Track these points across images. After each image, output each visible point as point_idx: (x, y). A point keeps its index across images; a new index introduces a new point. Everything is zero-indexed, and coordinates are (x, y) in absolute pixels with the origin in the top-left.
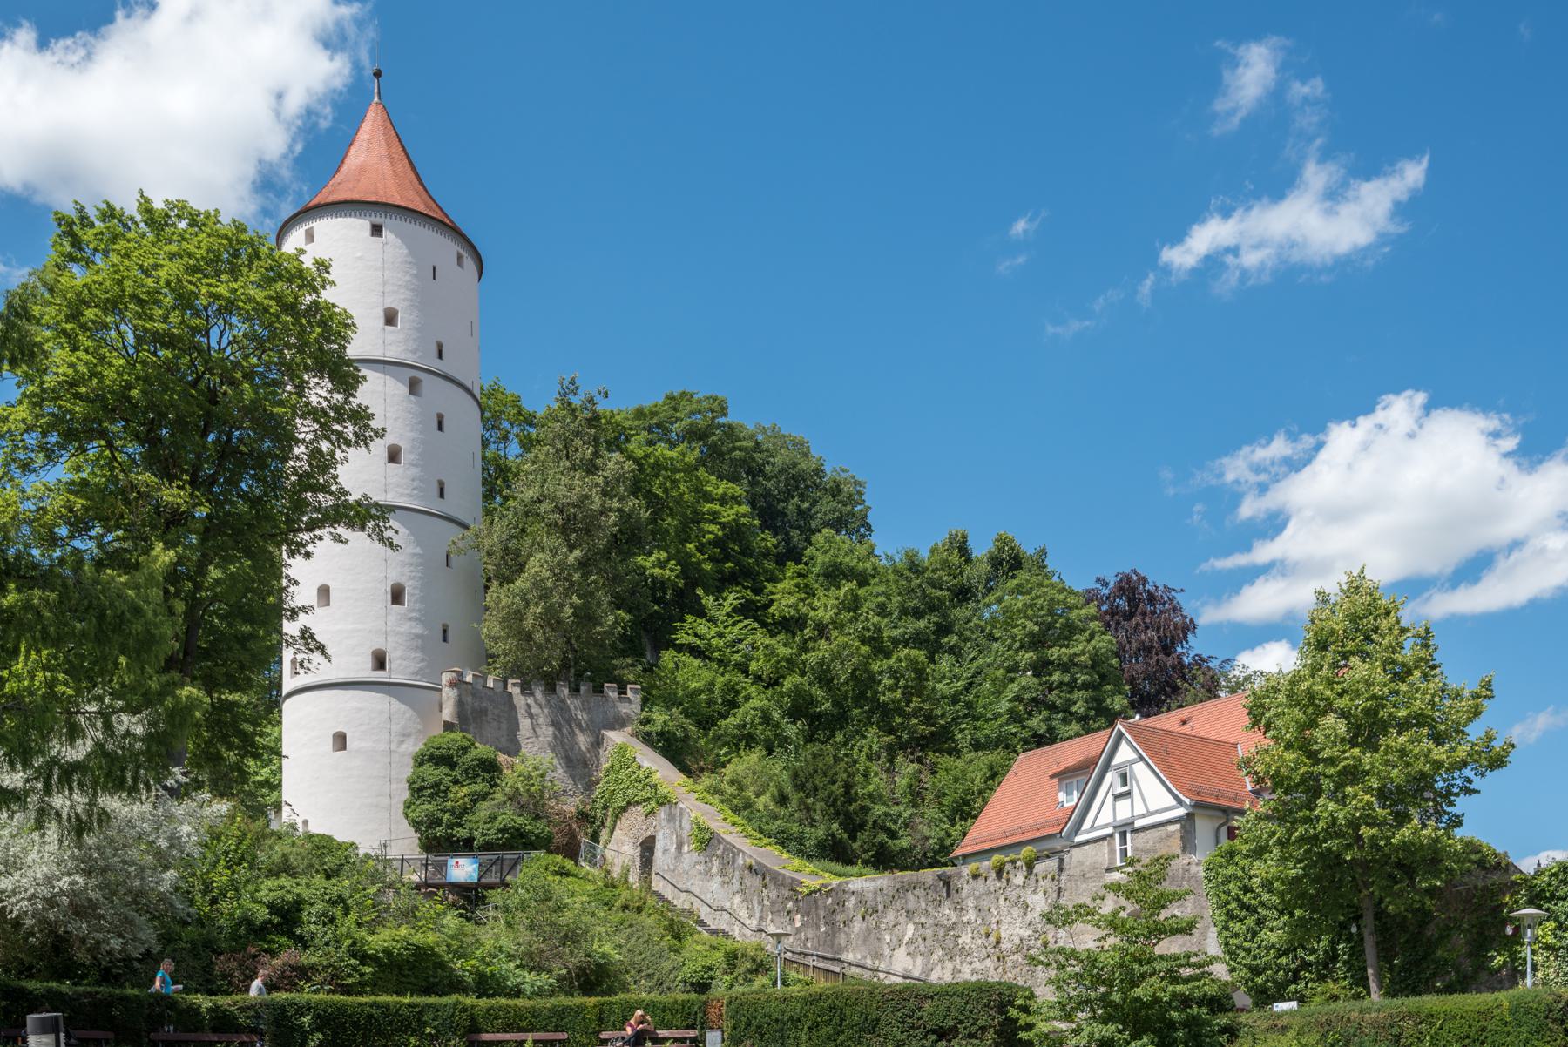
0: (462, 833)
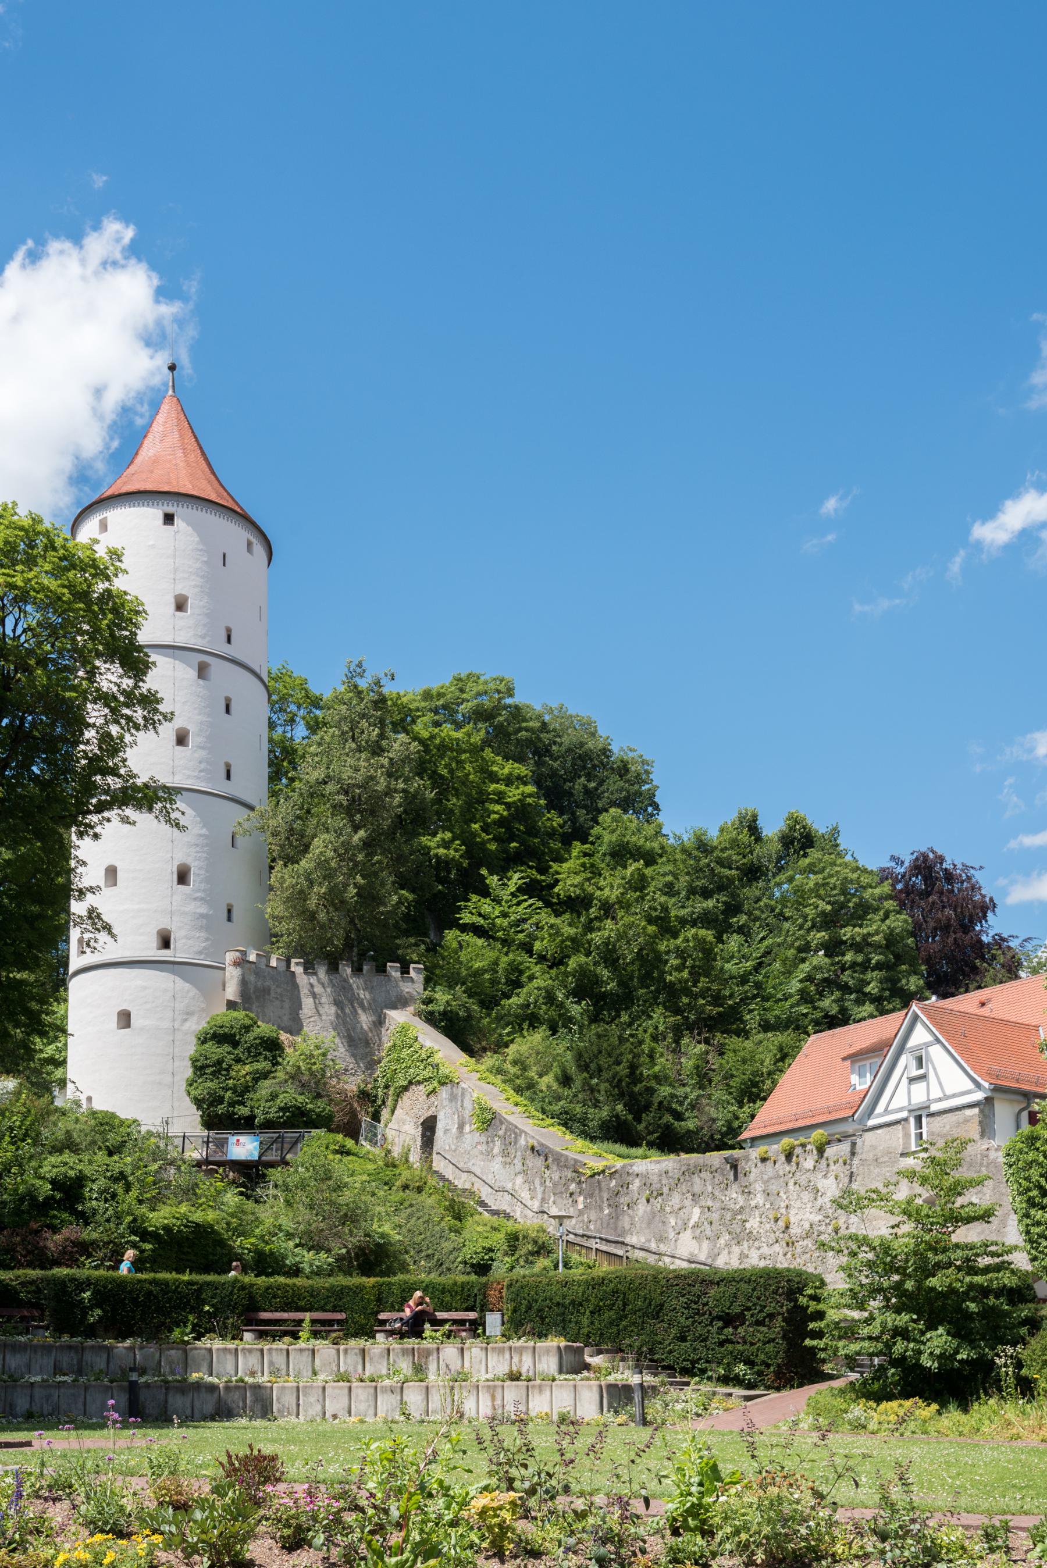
0: (243, 1111)
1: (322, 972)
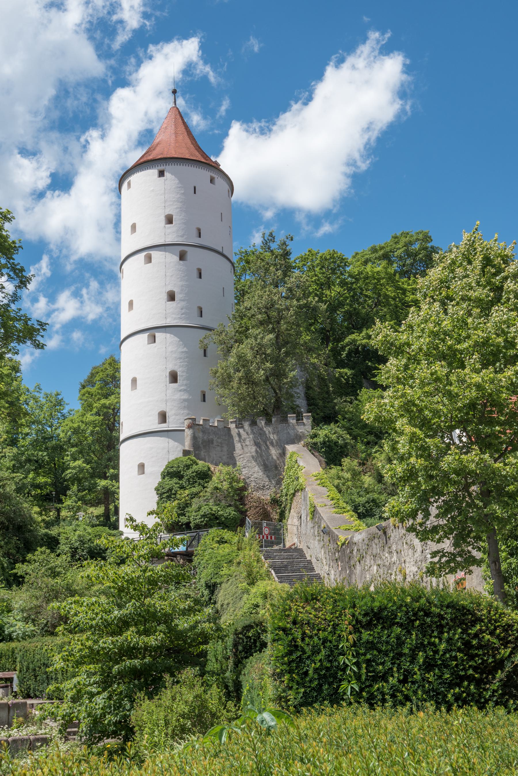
0: (184, 520)
1: (246, 425)
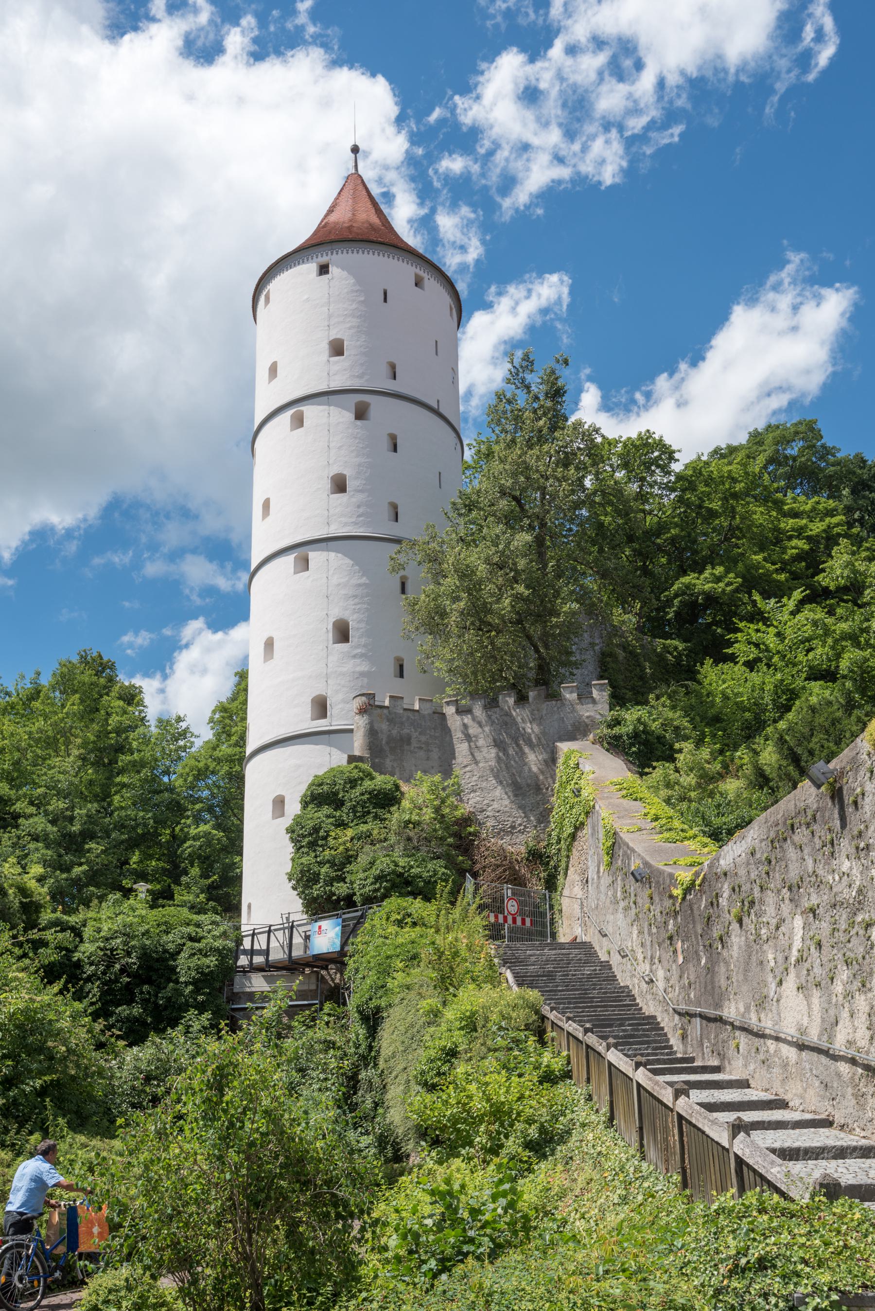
0: (341, 889)
1: (478, 710)
